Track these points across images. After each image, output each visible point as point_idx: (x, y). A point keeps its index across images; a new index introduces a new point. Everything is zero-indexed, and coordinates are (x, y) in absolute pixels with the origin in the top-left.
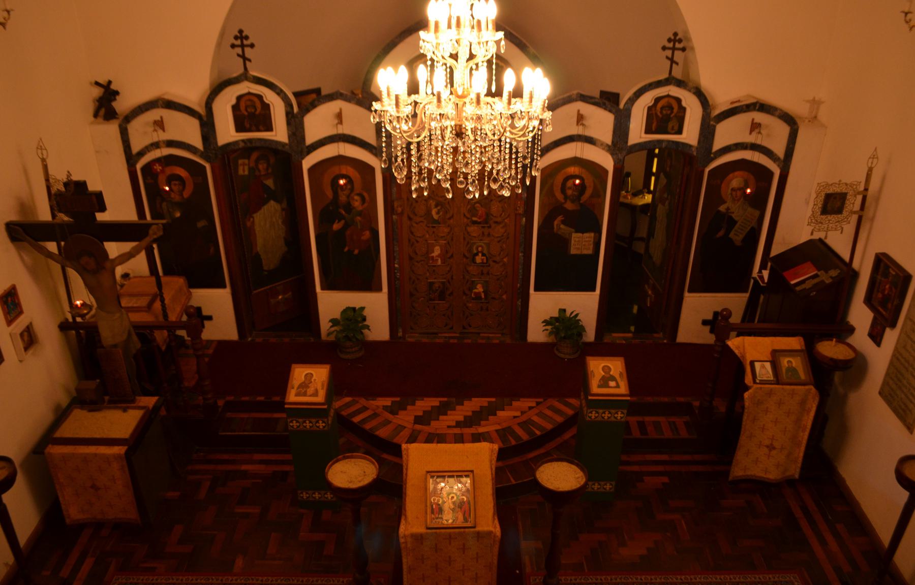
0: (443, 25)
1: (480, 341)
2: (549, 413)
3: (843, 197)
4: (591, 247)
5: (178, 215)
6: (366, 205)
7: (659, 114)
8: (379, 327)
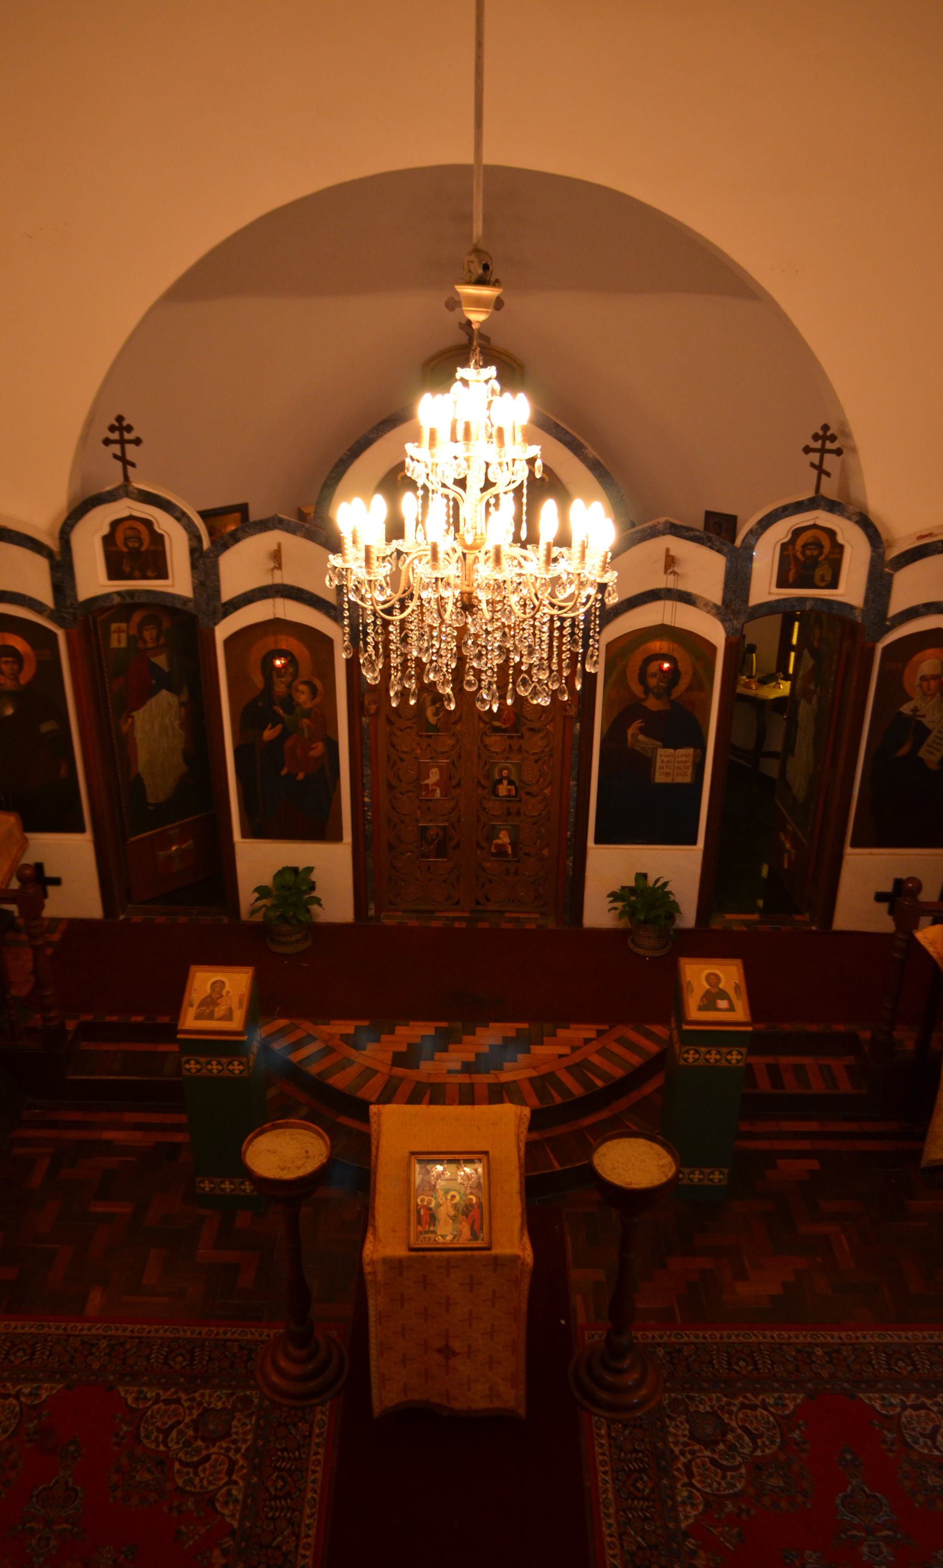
0: (443, 435)
2: (617, 1049)
4: (690, 771)
5: (9, 711)
6: (318, 699)
7: (799, 555)
8: (336, 900)
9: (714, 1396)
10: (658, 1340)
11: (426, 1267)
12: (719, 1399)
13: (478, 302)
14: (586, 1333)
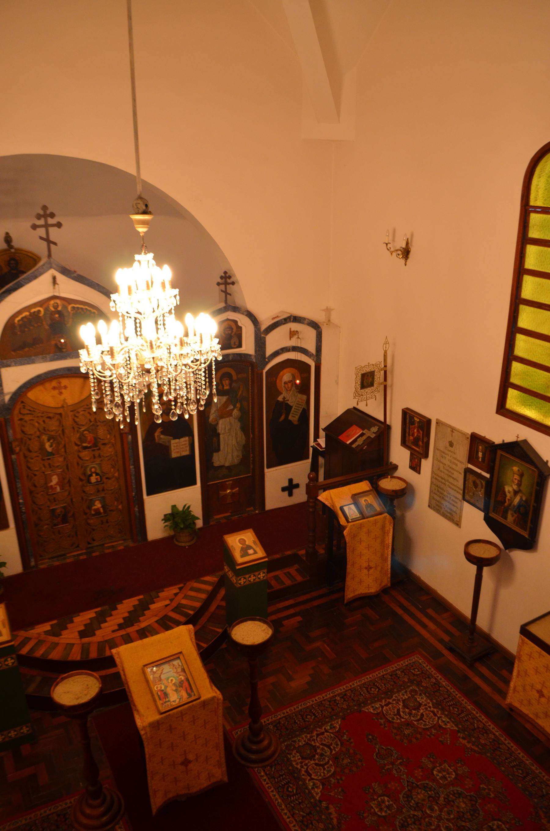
1: (107, 551)
3: (372, 374)
4: (188, 448)
9: (303, 736)
10: (267, 722)
11: (170, 720)
12: (306, 737)
13: (143, 223)
14: (233, 732)
